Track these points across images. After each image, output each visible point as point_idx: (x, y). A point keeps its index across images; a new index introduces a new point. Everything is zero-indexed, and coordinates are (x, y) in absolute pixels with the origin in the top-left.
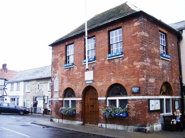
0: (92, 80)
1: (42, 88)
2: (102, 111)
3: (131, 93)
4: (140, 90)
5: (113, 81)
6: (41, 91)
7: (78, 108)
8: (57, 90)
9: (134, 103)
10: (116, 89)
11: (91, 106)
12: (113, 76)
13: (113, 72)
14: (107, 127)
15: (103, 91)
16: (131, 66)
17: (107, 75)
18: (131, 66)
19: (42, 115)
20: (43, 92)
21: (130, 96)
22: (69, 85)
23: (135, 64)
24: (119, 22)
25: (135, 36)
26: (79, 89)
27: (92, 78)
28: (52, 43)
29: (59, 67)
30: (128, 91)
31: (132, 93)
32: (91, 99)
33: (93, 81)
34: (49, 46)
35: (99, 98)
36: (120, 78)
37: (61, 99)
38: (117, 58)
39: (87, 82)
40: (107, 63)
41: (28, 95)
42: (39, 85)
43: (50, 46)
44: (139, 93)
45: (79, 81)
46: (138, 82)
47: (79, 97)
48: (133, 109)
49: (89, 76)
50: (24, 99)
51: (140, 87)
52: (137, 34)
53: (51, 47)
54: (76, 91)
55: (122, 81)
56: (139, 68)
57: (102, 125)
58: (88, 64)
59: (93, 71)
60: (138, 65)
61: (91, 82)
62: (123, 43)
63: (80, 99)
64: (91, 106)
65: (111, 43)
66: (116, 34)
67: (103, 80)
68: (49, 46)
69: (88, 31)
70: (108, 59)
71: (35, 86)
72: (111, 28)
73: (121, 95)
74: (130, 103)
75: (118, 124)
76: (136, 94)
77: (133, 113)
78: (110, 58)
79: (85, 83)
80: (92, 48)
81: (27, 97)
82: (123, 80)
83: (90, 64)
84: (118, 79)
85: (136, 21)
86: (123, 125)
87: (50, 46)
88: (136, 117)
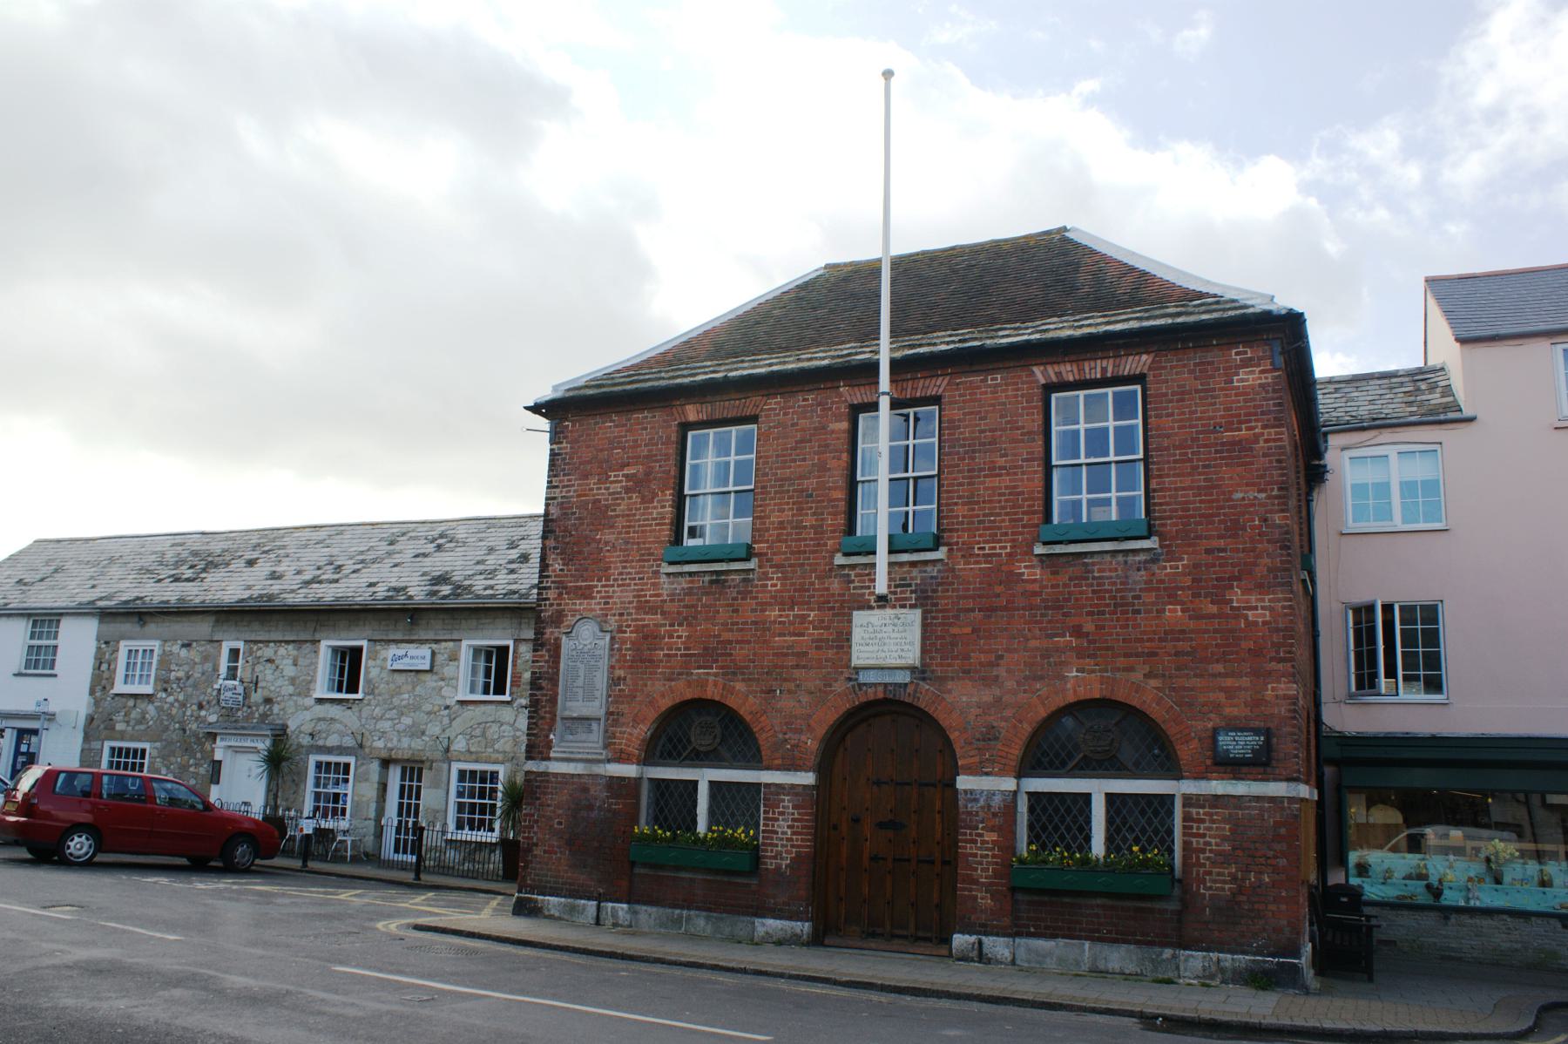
0: (912, 669)
1: (266, 673)
2: (979, 851)
3: (1209, 762)
4: (1267, 747)
5: (1079, 681)
6: (256, 697)
7: (784, 837)
8: (596, 708)
9: (1224, 821)
10: (1102, 731)
11: (881, 825)
12: (1081, 653)
13: (1077, 632)
14: (1021, 954)
15: (996, 739)
16: (1214, 609)
17: (1034, 643)
18: (1214, 609)
19: (409, 876)
20: (268, 701)
21: (1199, 776)
22: (702, 683)
23: (1237, 596)
24: (1126, 346)
25: (1233, 443)
26: (799, 713)
27: (913, 656)
28: (545, 393)
29: (614, 558)
30: (1186, 753)
31: (1216, 764)
32: (878, 783)
33: (920, 672)
34: (527, 408)
35: (964, 782)
36: (1130, 669)
37: (629, 770)
38: (1114, 553)
39: (864, 678)
40: (1029, 571)
41: (134, 714)
42: (234, 653)
43: (536, 409)
44: (1266, 764)
45: (797, 666)
46: (1257, 702)
47: (791, 766)
48: (1219, 853)
49: (886, 642)
50: (96, 745)
51: (1268, 733)
52: (1257, 436)
53: (544, 423)
54: (768, 730)
55: (1143, 689)
56: (1264, 623)
57: (980, 943)
58: (891, 564)
59: (918, 613)
60: (1256, 608)
61: (903, 678)
62: (753, 501)
63: (807, 778)
64: (881, 825)
65: (687, 491)
66: (723, 449)
67: (1001, 672)
68: (527, 408)
69: (894, 364)
70: (1039, 549)
71: (205, 659)
72: (1069, 372)
73: (1126, 768)
74: (1203, 821)
75: (1101, 940)
76: (1245, 769)
77: (1218, 874)
78: (1058, 549)
79: (850, 679)
80: (727, 485)
81: (120, 727)
82: (1153, 683)
83: (901, 564)
84: (1118, 675)
85: (1246, 363)
86: (1137, 943)
87: (536, 409)
88: (1244, 898)
